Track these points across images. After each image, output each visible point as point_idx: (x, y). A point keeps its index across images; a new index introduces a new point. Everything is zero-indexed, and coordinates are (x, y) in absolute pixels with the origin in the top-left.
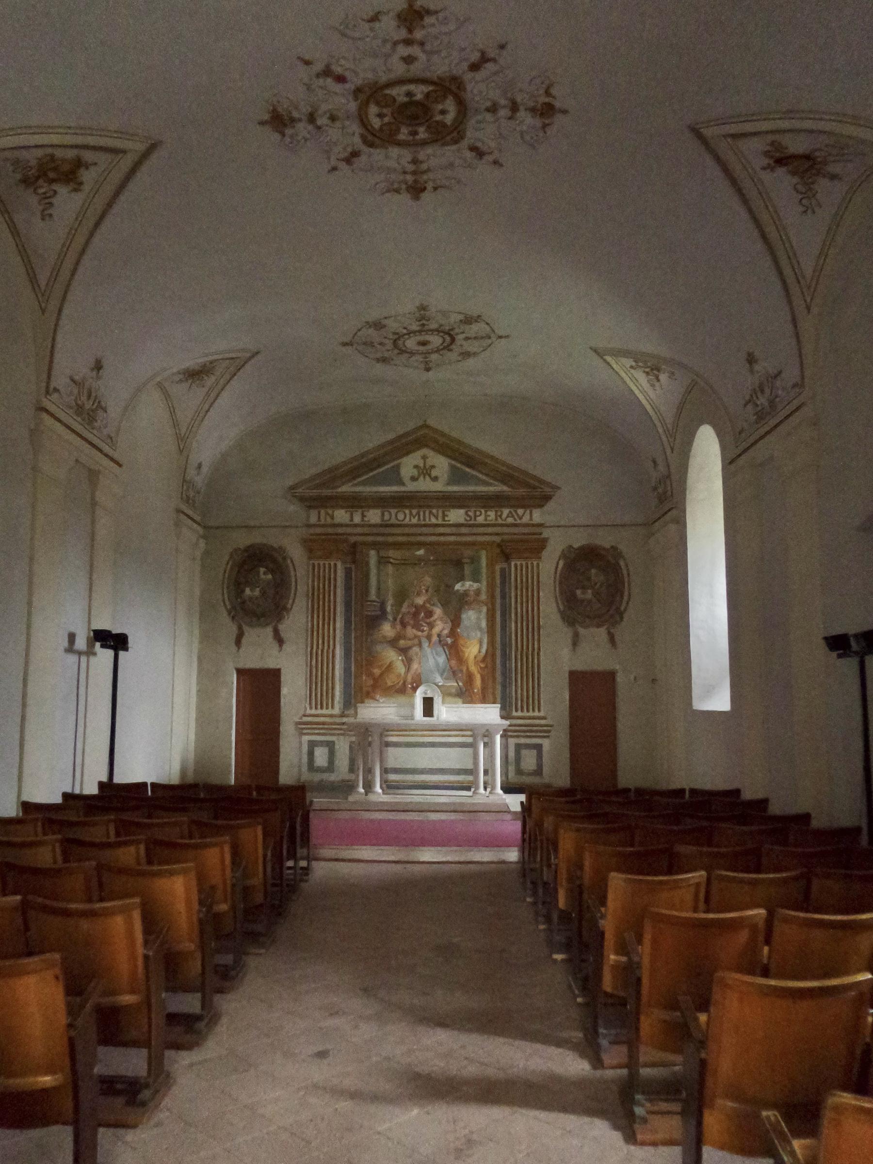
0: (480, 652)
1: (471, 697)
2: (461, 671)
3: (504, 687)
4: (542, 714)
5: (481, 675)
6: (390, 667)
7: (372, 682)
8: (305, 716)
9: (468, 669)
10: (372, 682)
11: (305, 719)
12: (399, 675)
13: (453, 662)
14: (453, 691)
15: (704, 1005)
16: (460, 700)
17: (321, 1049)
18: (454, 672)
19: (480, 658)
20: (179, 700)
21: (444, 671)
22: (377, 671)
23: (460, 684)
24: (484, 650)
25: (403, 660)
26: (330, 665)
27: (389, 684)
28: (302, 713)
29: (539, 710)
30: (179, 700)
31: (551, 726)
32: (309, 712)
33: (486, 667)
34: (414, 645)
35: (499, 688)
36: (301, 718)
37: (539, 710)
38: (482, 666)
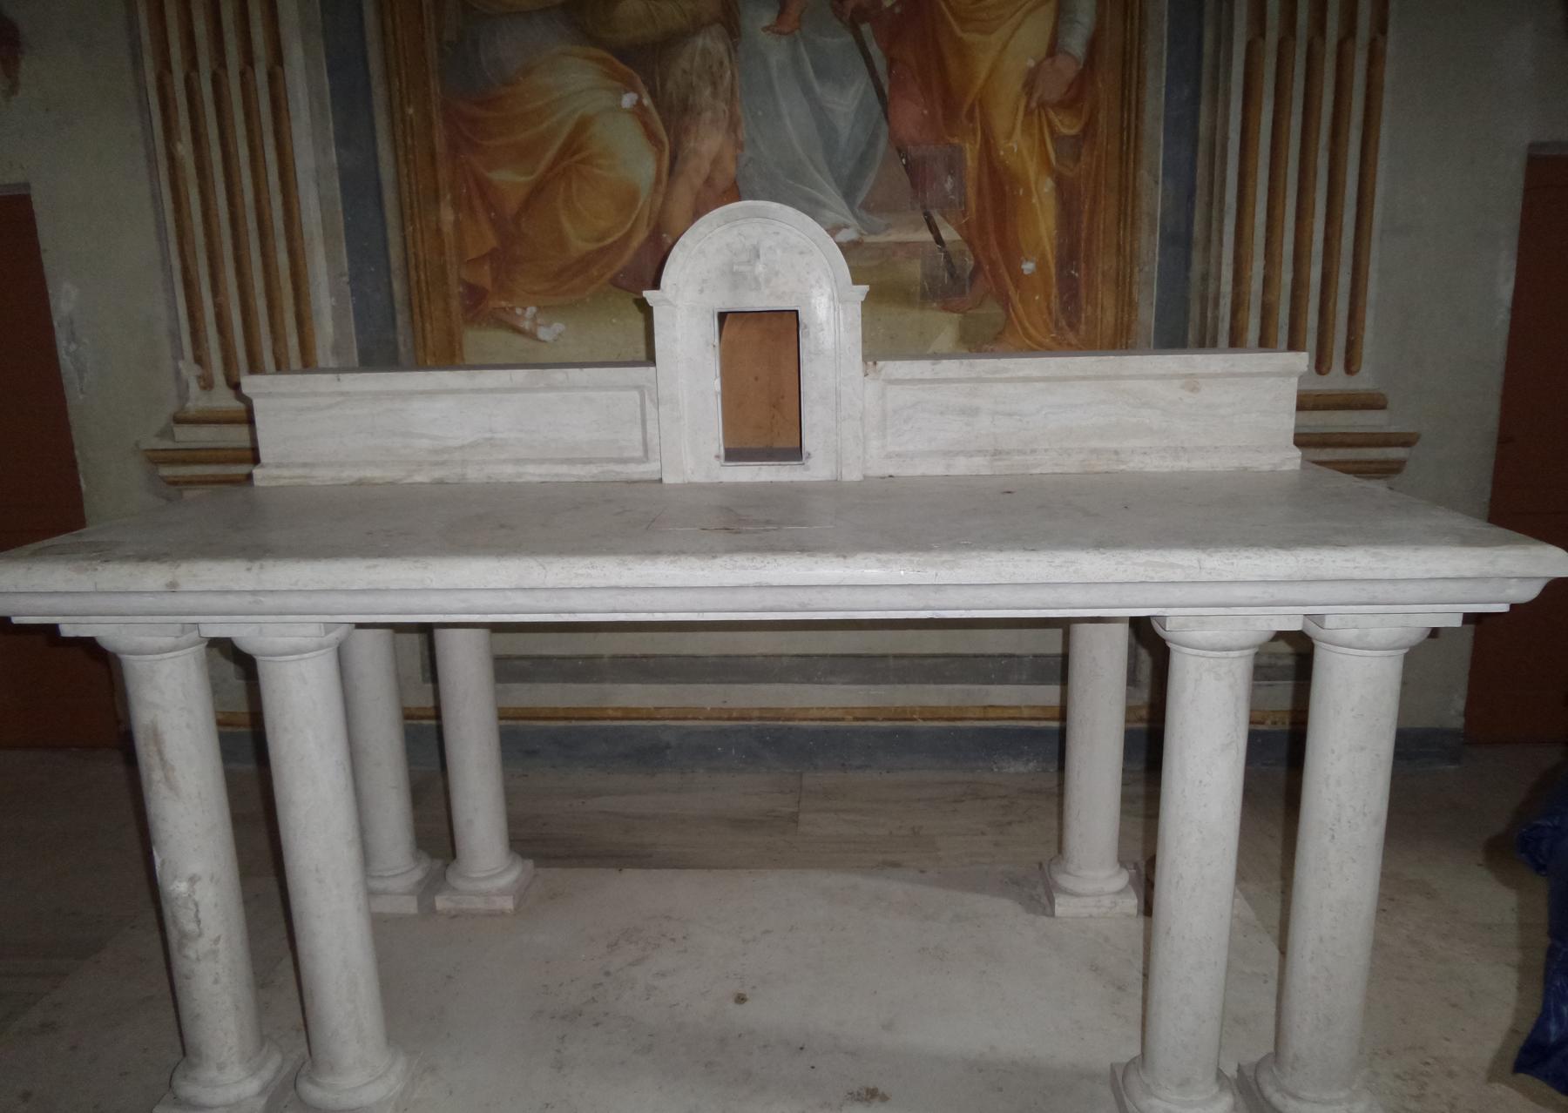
0: (1053, 49)
1: (1005, 301)
2: (954, 166)
3: (1179, 241)
4: (1363, 382)
5: (1060, 182)
6: (576, 149)
7: (492, 241)
8: (179, 420)
9: (988, 146)
10: (492, 241)
11: (191, 436)
12: (627, 200)
13: (911, 114)
14: (914, 270)
15: (656, 285)
16: (945, 326)
17: (891, 471)
18: (916, 172)
19: (1053, 89)
20: (563, 469)
21: (863, 161)
22: (511, 180)
23: (949, 233)
24: (1076, 44)
25: (639, 111)
26: (271, 155)
27: (579, 244)
28: (171, 408)
29: (1350, 367)
30: (563, 469)
31: (1407, 441)
32: (198, 401)
33: (1089, 131)
34: (697, 26)
35: (1149, 245)
36: (165, 433)
37: (1350, 367)
38: (1068, 126)
